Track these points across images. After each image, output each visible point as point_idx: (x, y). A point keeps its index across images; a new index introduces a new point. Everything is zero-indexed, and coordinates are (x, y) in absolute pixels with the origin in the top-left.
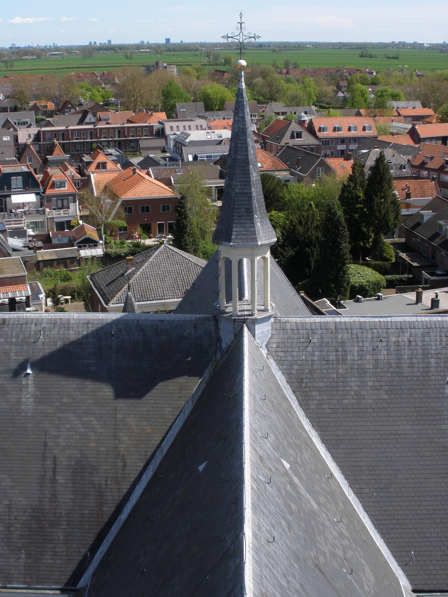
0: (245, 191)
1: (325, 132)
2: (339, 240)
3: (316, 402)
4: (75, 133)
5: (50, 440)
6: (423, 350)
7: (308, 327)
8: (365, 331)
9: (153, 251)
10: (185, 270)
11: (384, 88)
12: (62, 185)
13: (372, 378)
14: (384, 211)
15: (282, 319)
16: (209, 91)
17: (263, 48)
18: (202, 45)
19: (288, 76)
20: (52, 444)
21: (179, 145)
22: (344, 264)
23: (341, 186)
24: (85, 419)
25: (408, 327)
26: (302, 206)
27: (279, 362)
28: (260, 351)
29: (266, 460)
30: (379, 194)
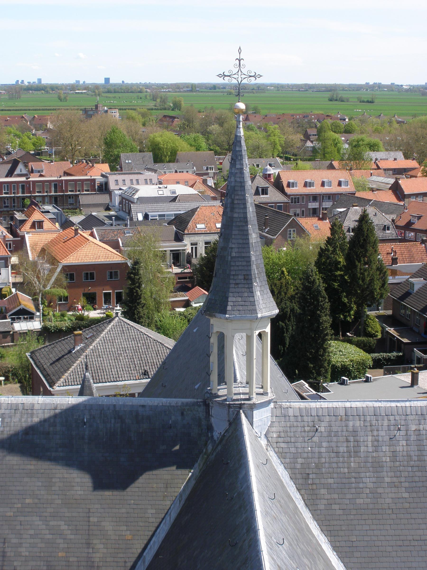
0: (243, 255)
1: (295, 188)
2: (318, 312)
3: (325, 502)
4: (5, 186)
5: (10, 549)
8: (380, 418)
9: (106, 325)
10: (142, 347)
11: (360, 137)
13: (389, 474)
14: (368, 279)
15: (284, 404)
16: (159, 139)
17: (217, 90)
18: (147, 86)
20: (12, 554)
21: (126, 202)
22: (324, 340)
23: (317, 250)
24: (52, 523)
25: (310, 415)
26: (271, 274)
27: (281, 455)
28: (259, 442)
30: (362, 259)
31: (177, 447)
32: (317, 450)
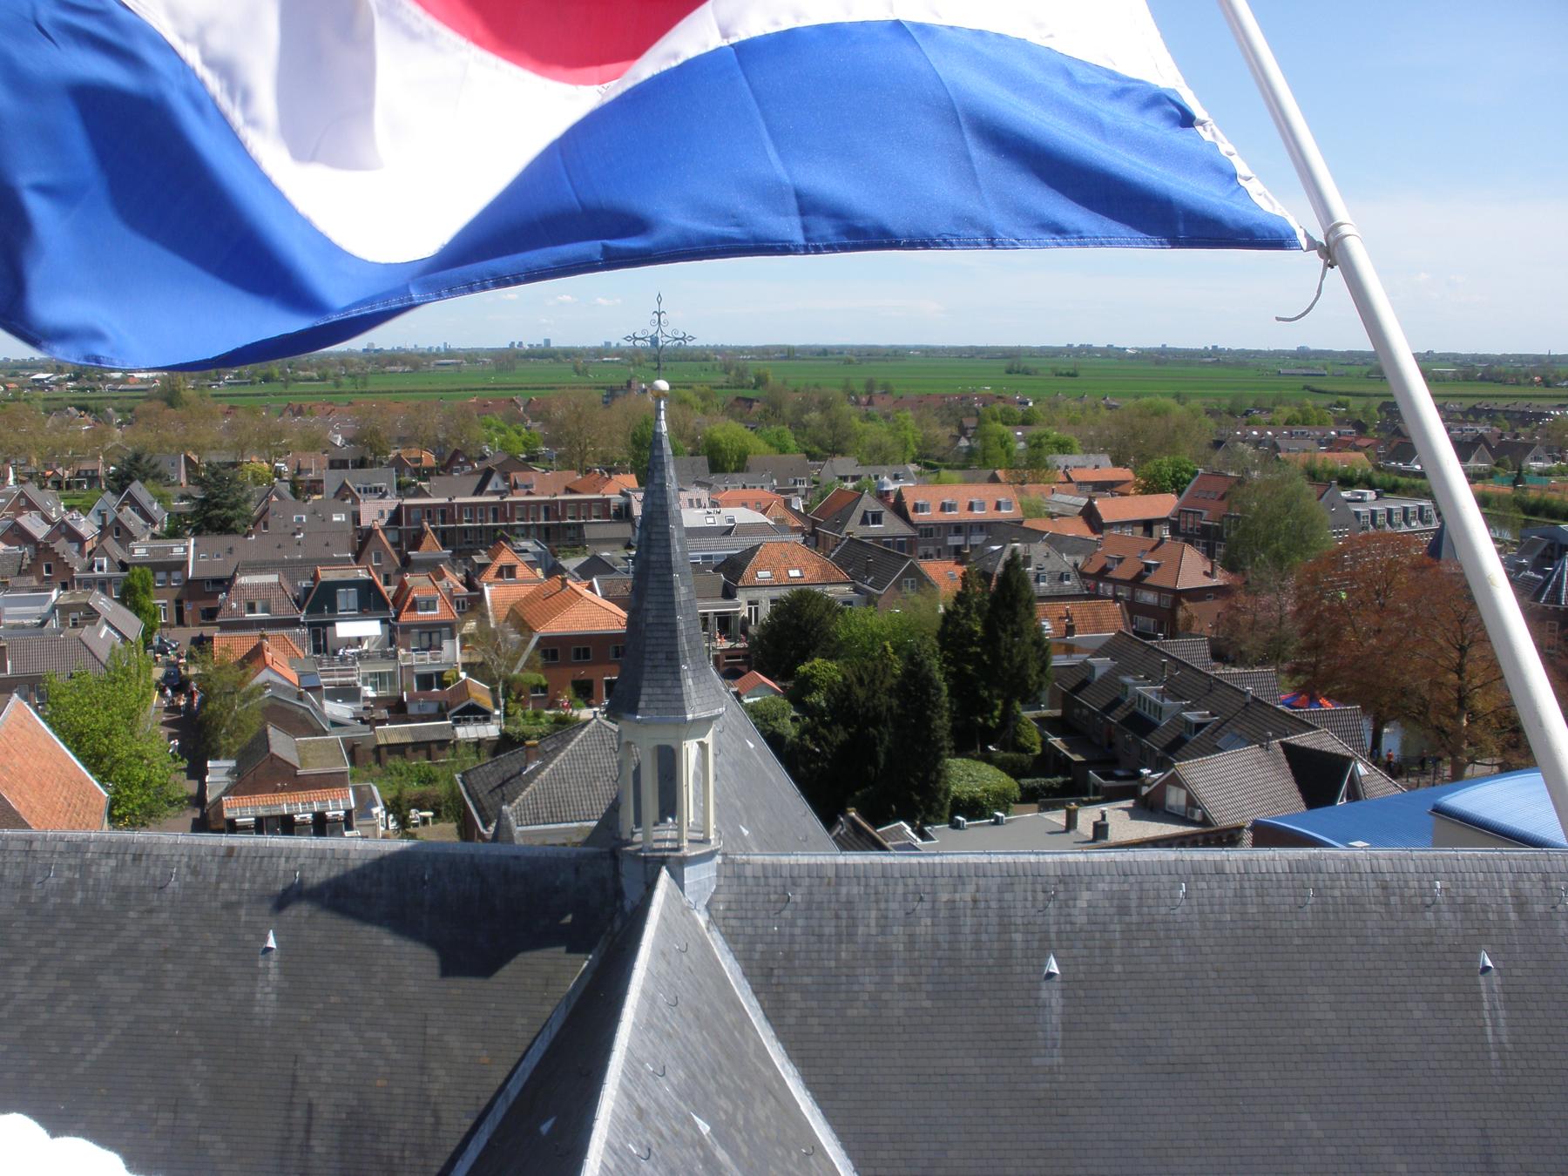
6: (1001, 917)
7: (785, 873)
8: (891, 881)
12: (430, 605)
16: (719, 435)
19: (870, 409)
20: (307, 1080)
22: (938, 758)
27: (730, 938)
29: (653, 1116)
31: (569, 919)
32: (787, 930)
